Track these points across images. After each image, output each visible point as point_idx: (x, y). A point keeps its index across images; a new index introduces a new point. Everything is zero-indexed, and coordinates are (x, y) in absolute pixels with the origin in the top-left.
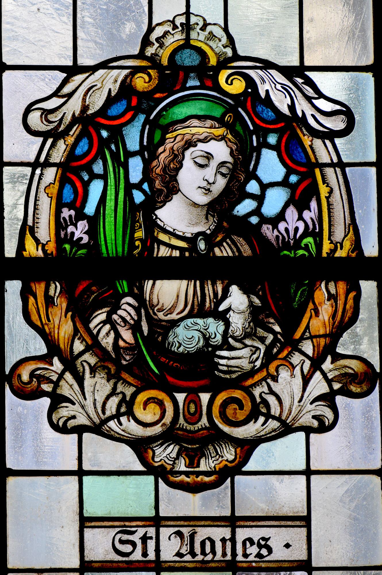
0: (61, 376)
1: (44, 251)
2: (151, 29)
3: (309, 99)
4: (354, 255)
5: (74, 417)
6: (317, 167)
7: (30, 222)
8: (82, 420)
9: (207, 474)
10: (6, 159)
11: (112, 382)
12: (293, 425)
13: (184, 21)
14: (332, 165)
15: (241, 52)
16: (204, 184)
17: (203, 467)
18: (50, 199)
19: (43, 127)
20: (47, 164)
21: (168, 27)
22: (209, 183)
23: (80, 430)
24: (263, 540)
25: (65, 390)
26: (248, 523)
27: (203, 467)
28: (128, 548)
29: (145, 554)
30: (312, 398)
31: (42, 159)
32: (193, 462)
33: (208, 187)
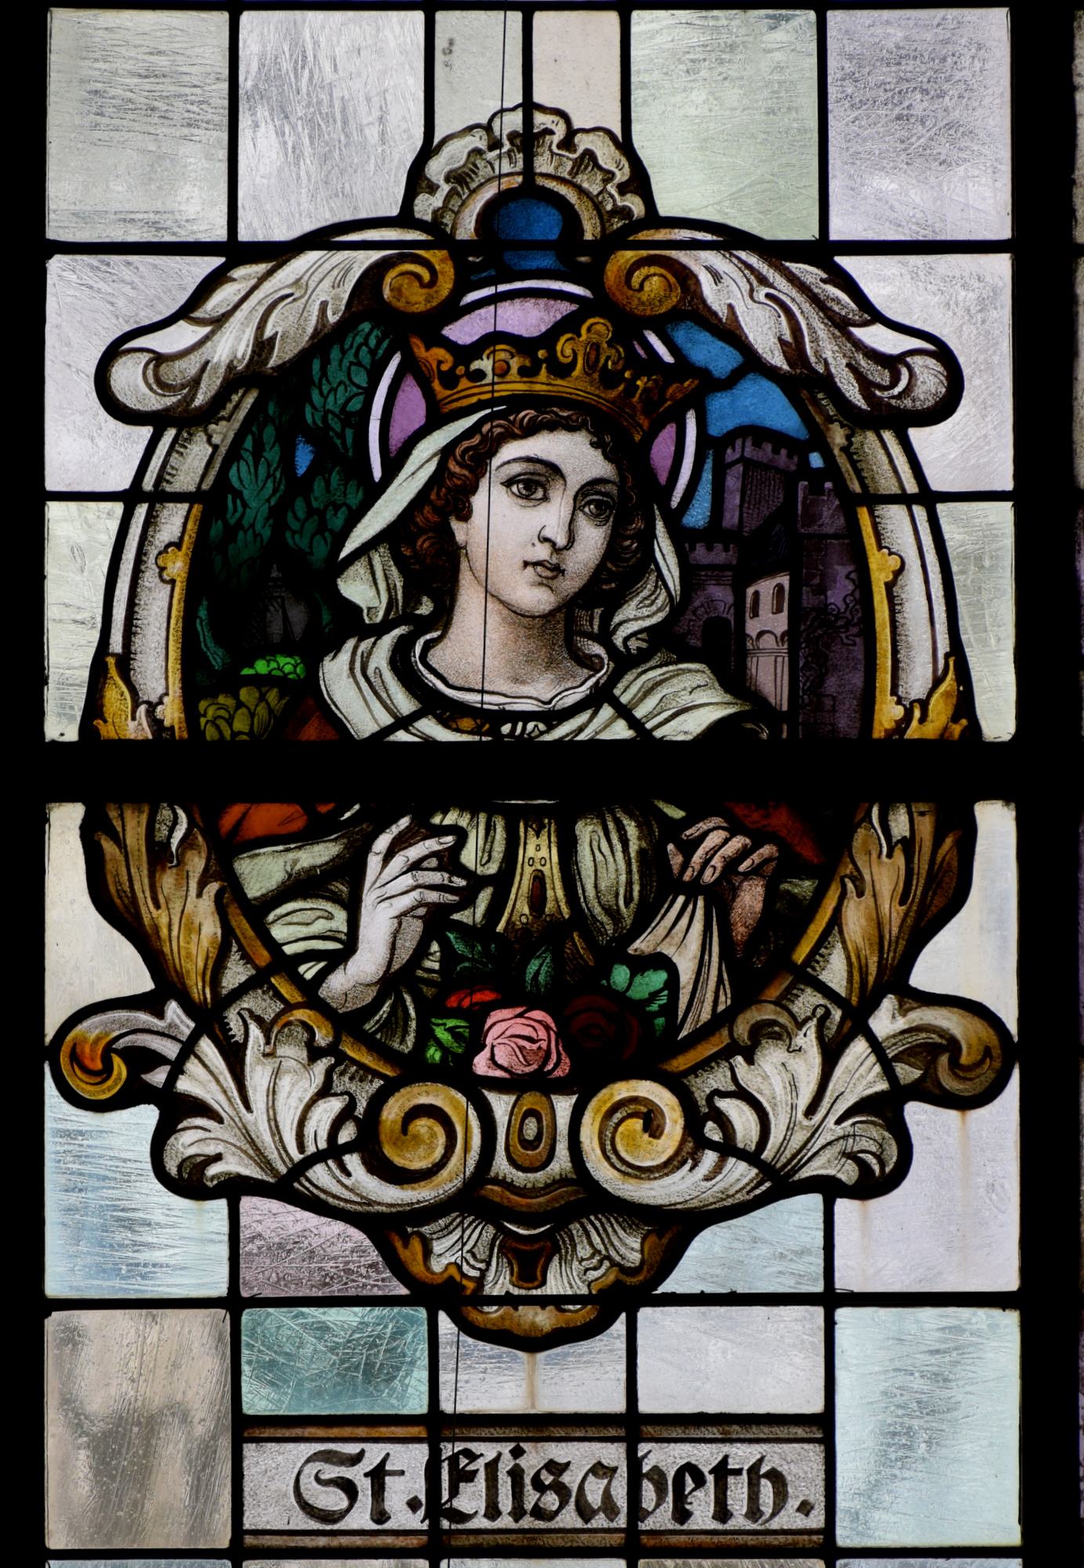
0: (188, 1049)
1: (156, 723)
2: (428, 150)
3: (841, 325)
4: (957, 730)
5: (218, 1158)
6: (861, 505)
7: (116, 644)
8: (235, 1164)
9: (557, 1302)
10: (51, 484)
11: (322, 1066)
12: (796, 1170)
13: (519, 128)
14: (903, 499)
15: (666, 207)
16: (543, 552)
17: (556, 1283)
18: (169, 587)
19: (154, 402)
20: (160, 497)
21: (478, 141)
22: (556, 549)
23: (234, 1189)
24: (550, 1472)
25: (193, 1083)
26: (287, 1433)
27: (556, 1283)
28: (334, 1500)
29: (722, 1512)
30: (841, 1107)
31: (148, 484)
32: (530, 1268)
33: (554, 561)
